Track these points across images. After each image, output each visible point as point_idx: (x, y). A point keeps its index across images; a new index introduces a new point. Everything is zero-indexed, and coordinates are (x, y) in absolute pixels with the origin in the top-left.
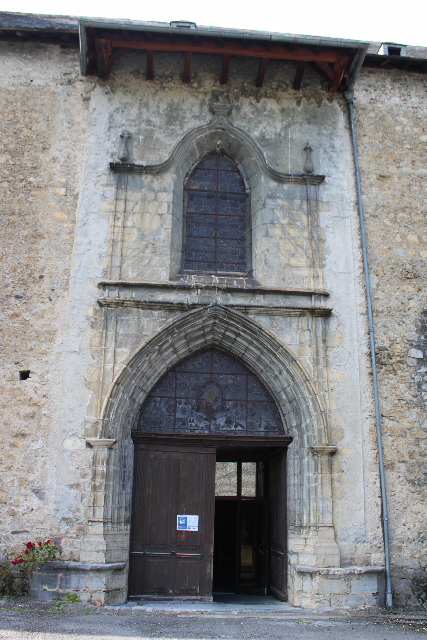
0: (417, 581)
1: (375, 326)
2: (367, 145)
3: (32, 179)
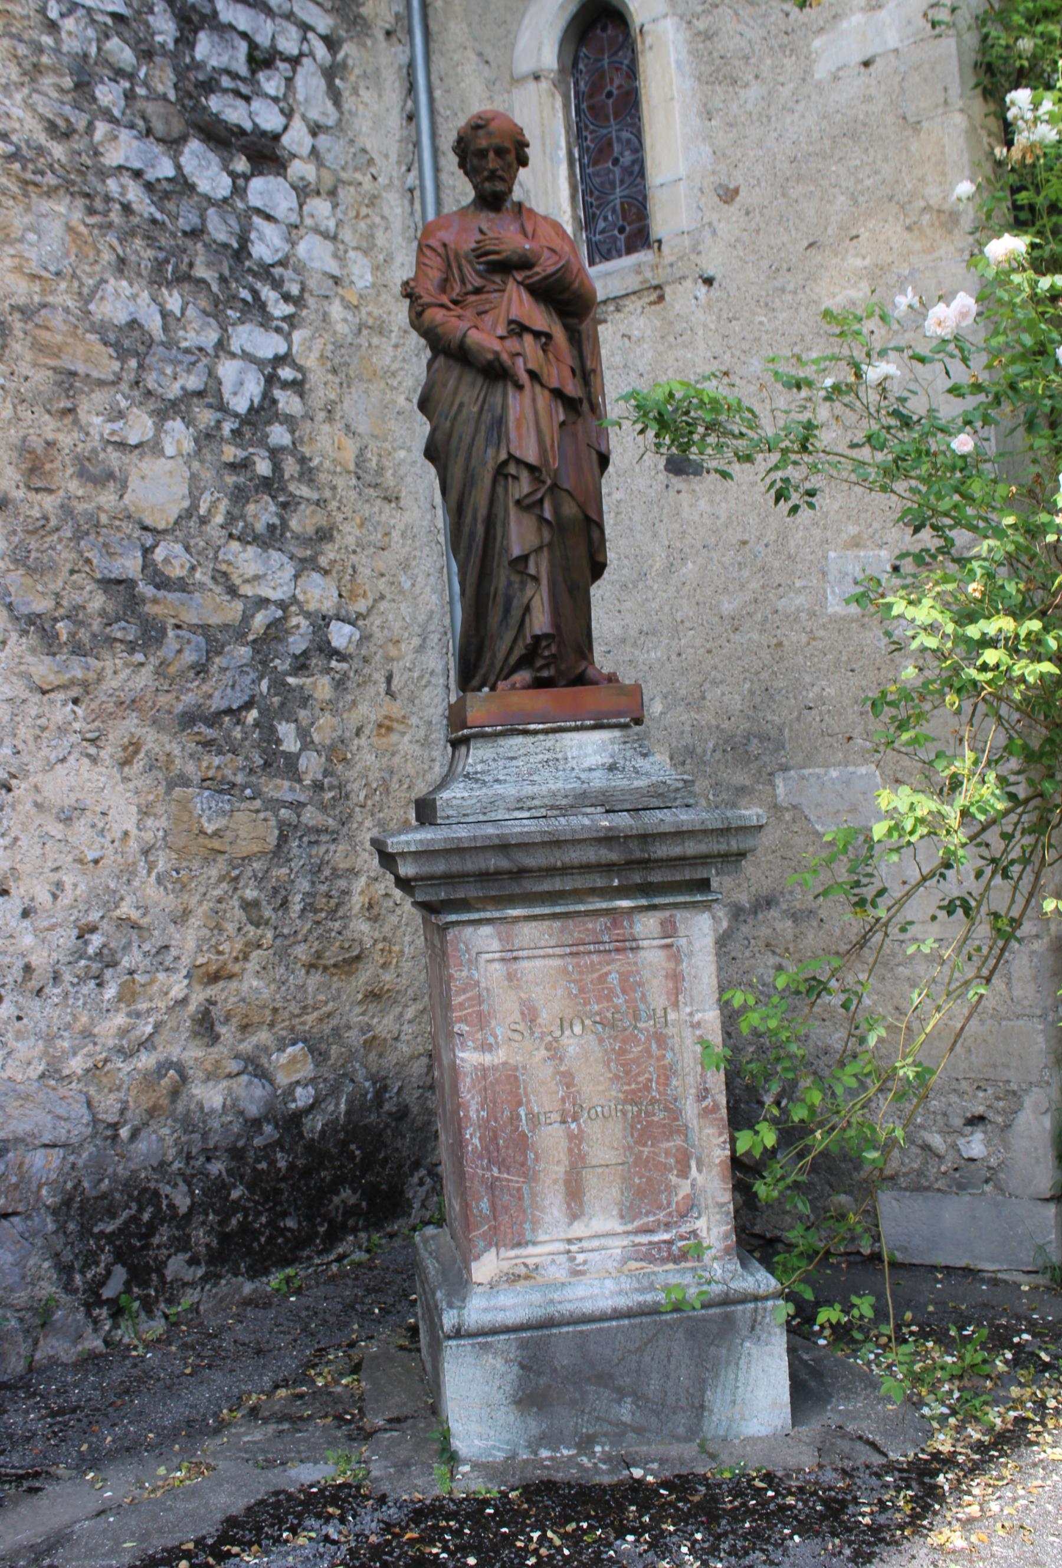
0: (82, 1211)
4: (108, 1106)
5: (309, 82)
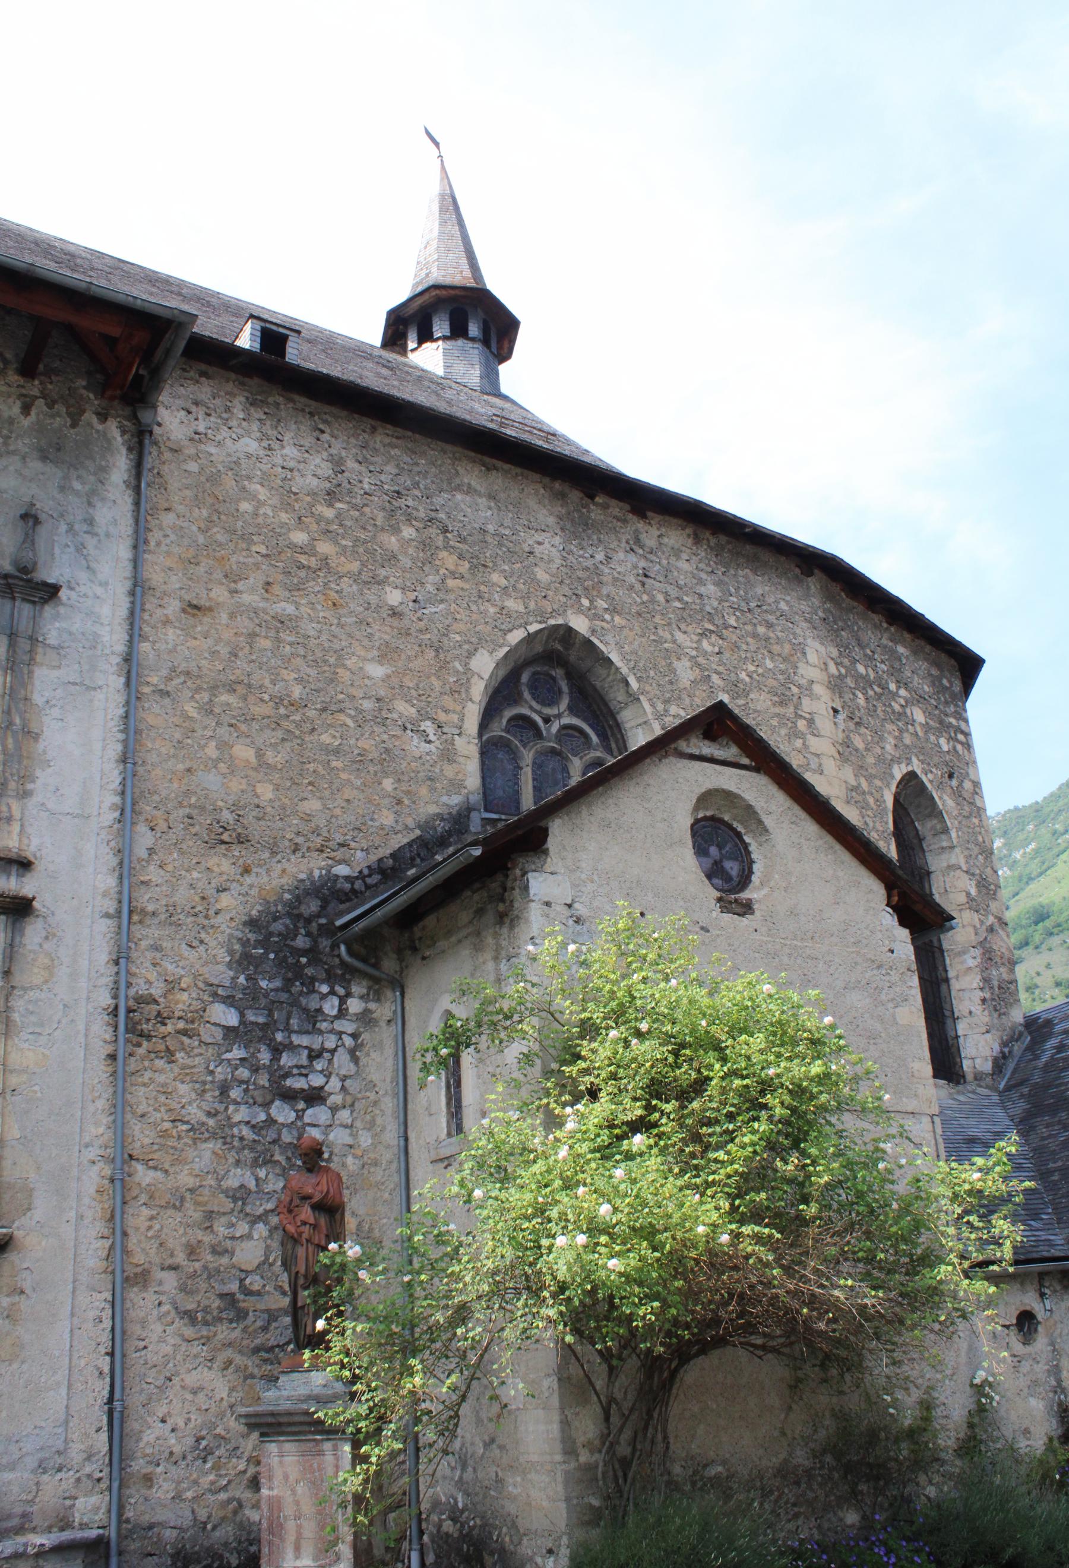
1: (133, 946)
2: (169, 532)
4: (202, 1514)
5: (342, 1059)
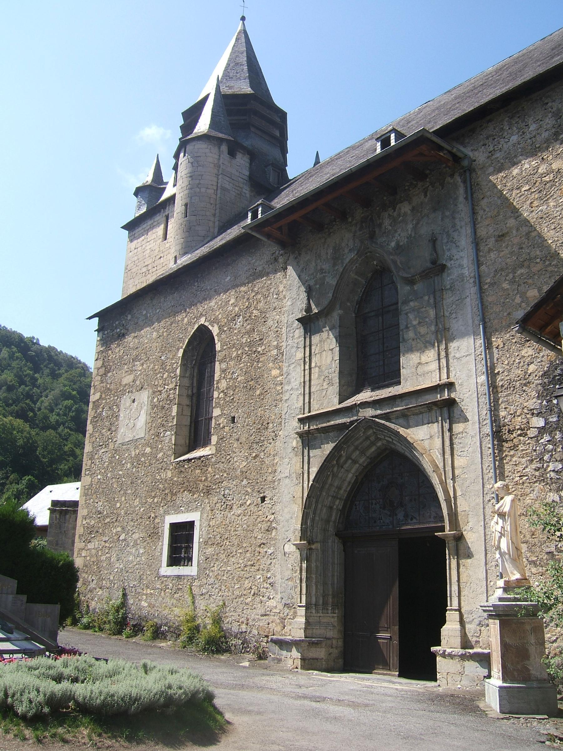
3: (259, 349)
